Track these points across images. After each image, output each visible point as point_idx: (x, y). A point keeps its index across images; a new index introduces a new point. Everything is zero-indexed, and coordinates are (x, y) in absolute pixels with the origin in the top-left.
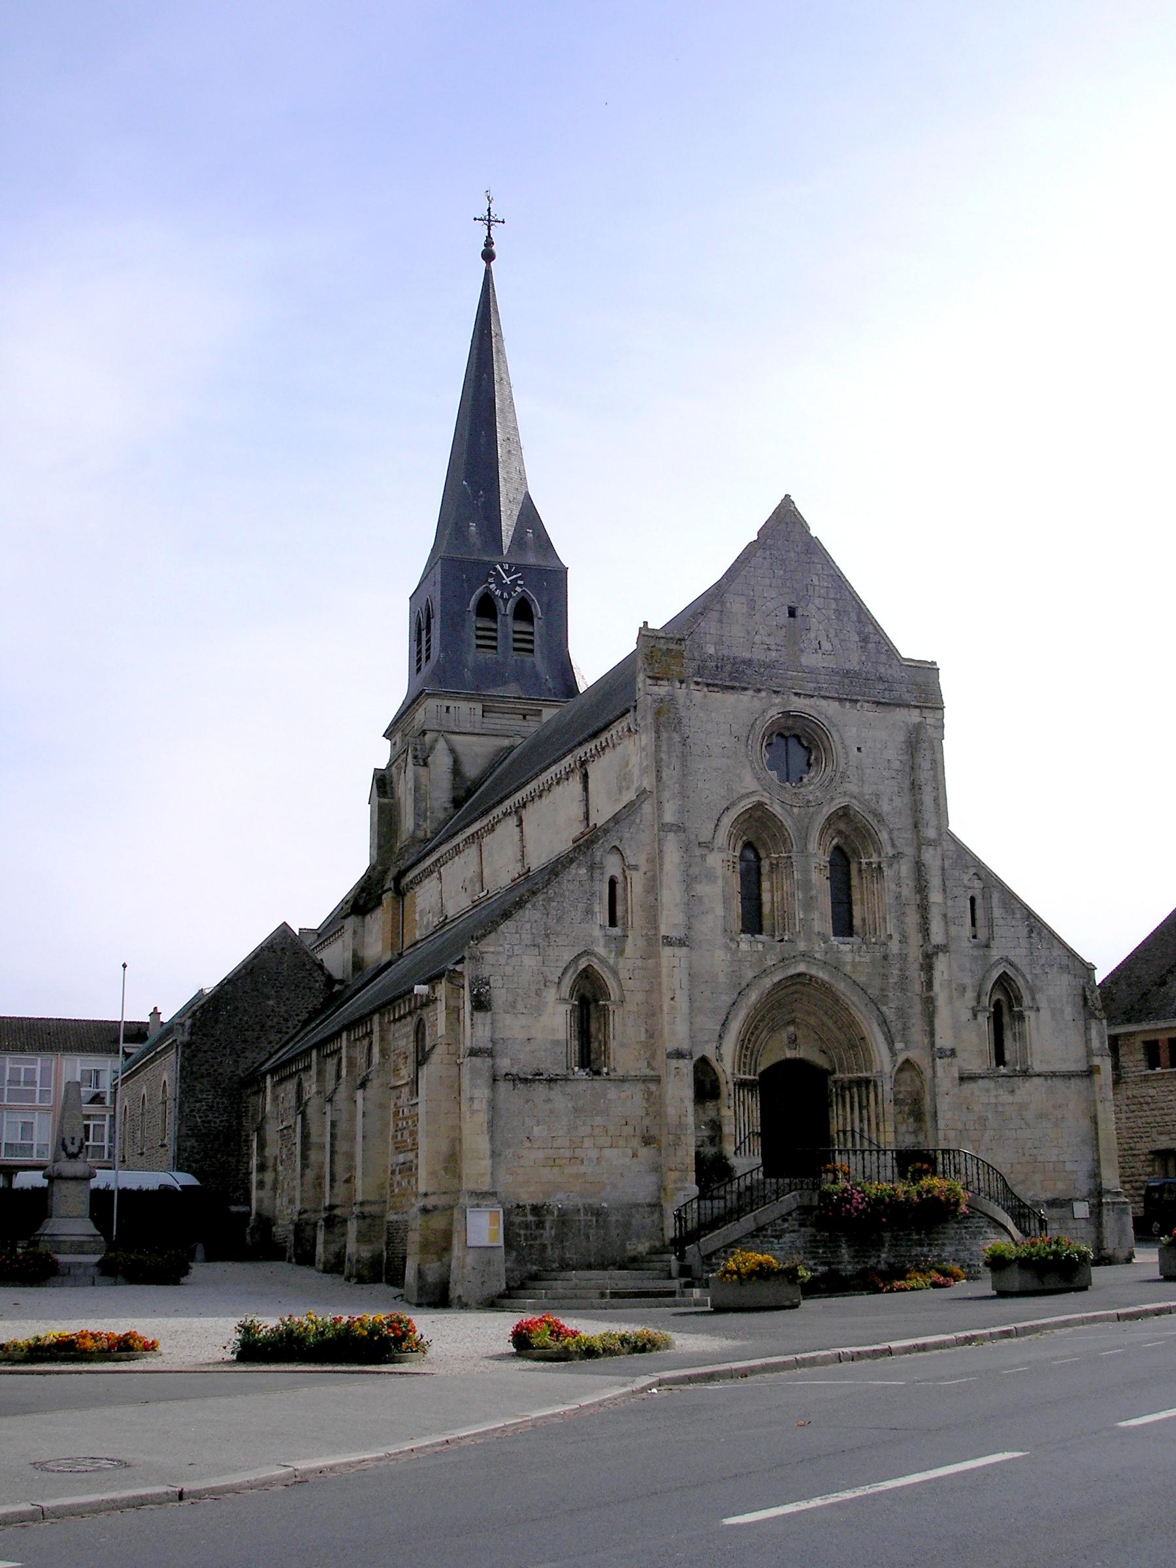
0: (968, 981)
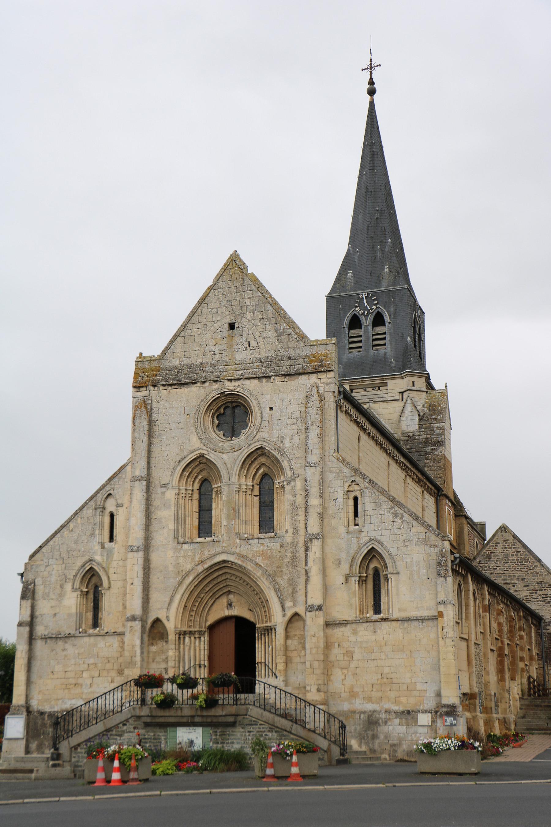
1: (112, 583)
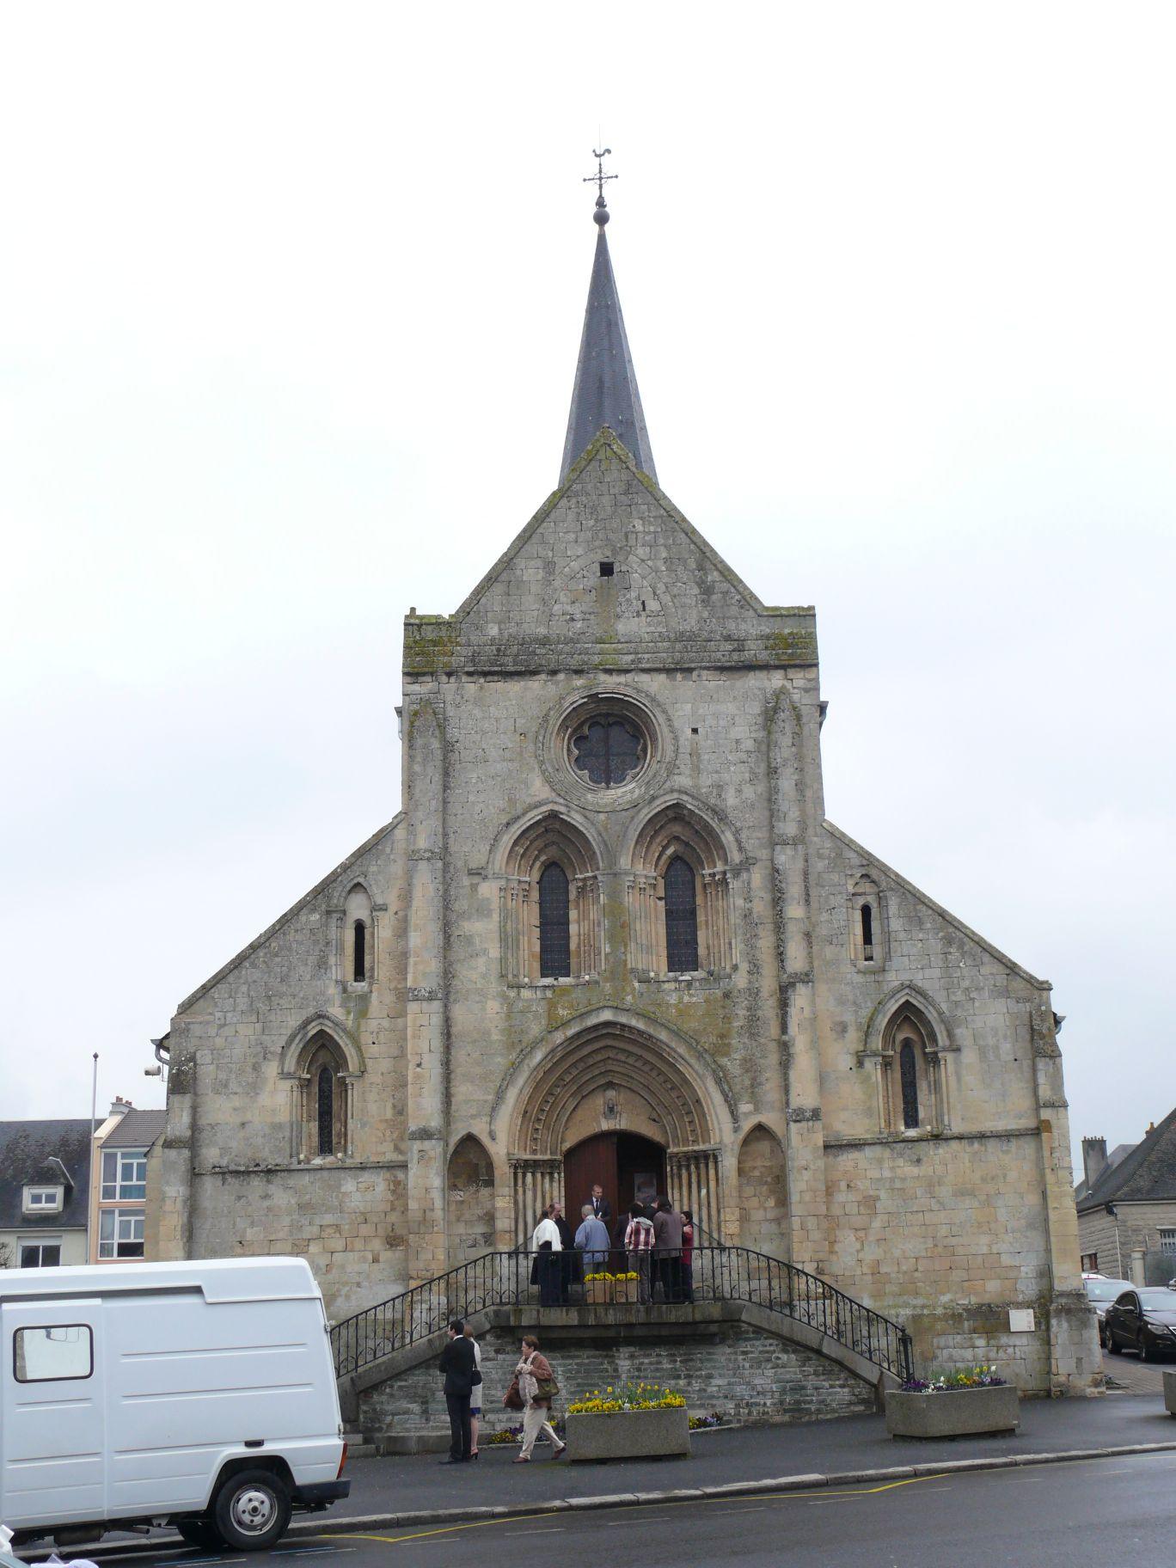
0: (849, 1017)
1: (369, 1063)
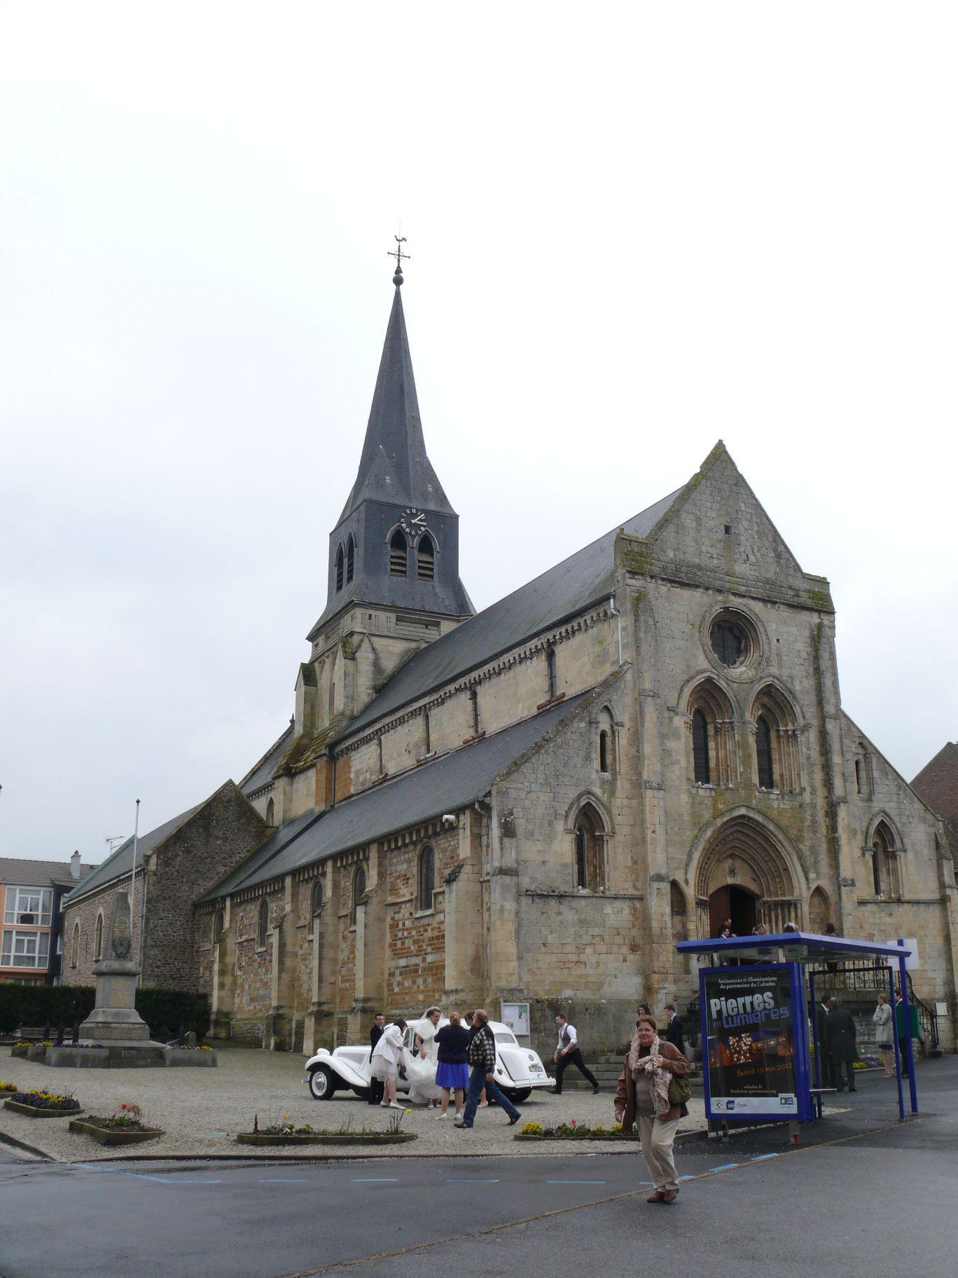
0: (857, 826)
